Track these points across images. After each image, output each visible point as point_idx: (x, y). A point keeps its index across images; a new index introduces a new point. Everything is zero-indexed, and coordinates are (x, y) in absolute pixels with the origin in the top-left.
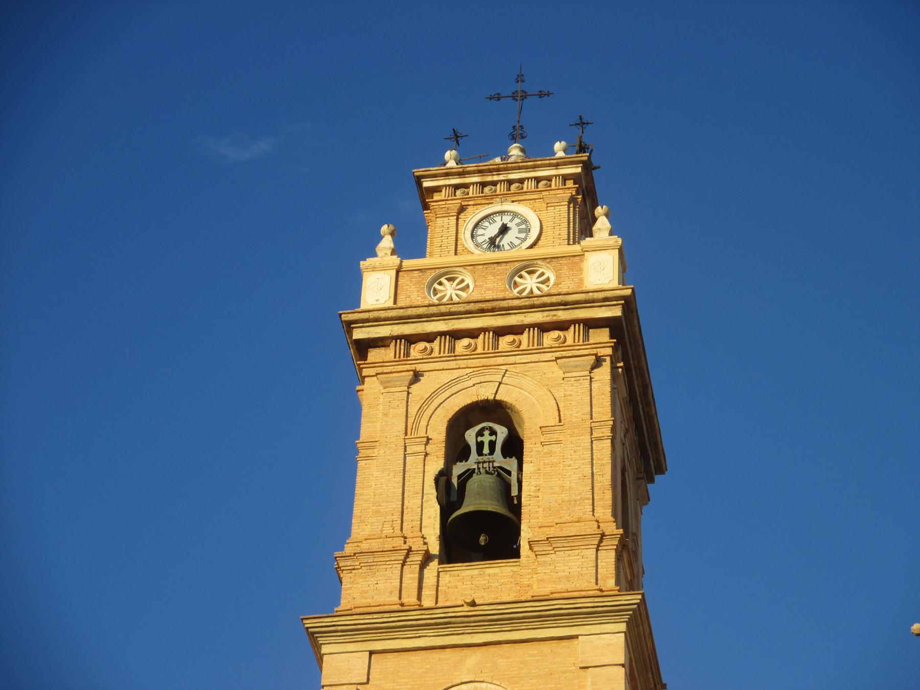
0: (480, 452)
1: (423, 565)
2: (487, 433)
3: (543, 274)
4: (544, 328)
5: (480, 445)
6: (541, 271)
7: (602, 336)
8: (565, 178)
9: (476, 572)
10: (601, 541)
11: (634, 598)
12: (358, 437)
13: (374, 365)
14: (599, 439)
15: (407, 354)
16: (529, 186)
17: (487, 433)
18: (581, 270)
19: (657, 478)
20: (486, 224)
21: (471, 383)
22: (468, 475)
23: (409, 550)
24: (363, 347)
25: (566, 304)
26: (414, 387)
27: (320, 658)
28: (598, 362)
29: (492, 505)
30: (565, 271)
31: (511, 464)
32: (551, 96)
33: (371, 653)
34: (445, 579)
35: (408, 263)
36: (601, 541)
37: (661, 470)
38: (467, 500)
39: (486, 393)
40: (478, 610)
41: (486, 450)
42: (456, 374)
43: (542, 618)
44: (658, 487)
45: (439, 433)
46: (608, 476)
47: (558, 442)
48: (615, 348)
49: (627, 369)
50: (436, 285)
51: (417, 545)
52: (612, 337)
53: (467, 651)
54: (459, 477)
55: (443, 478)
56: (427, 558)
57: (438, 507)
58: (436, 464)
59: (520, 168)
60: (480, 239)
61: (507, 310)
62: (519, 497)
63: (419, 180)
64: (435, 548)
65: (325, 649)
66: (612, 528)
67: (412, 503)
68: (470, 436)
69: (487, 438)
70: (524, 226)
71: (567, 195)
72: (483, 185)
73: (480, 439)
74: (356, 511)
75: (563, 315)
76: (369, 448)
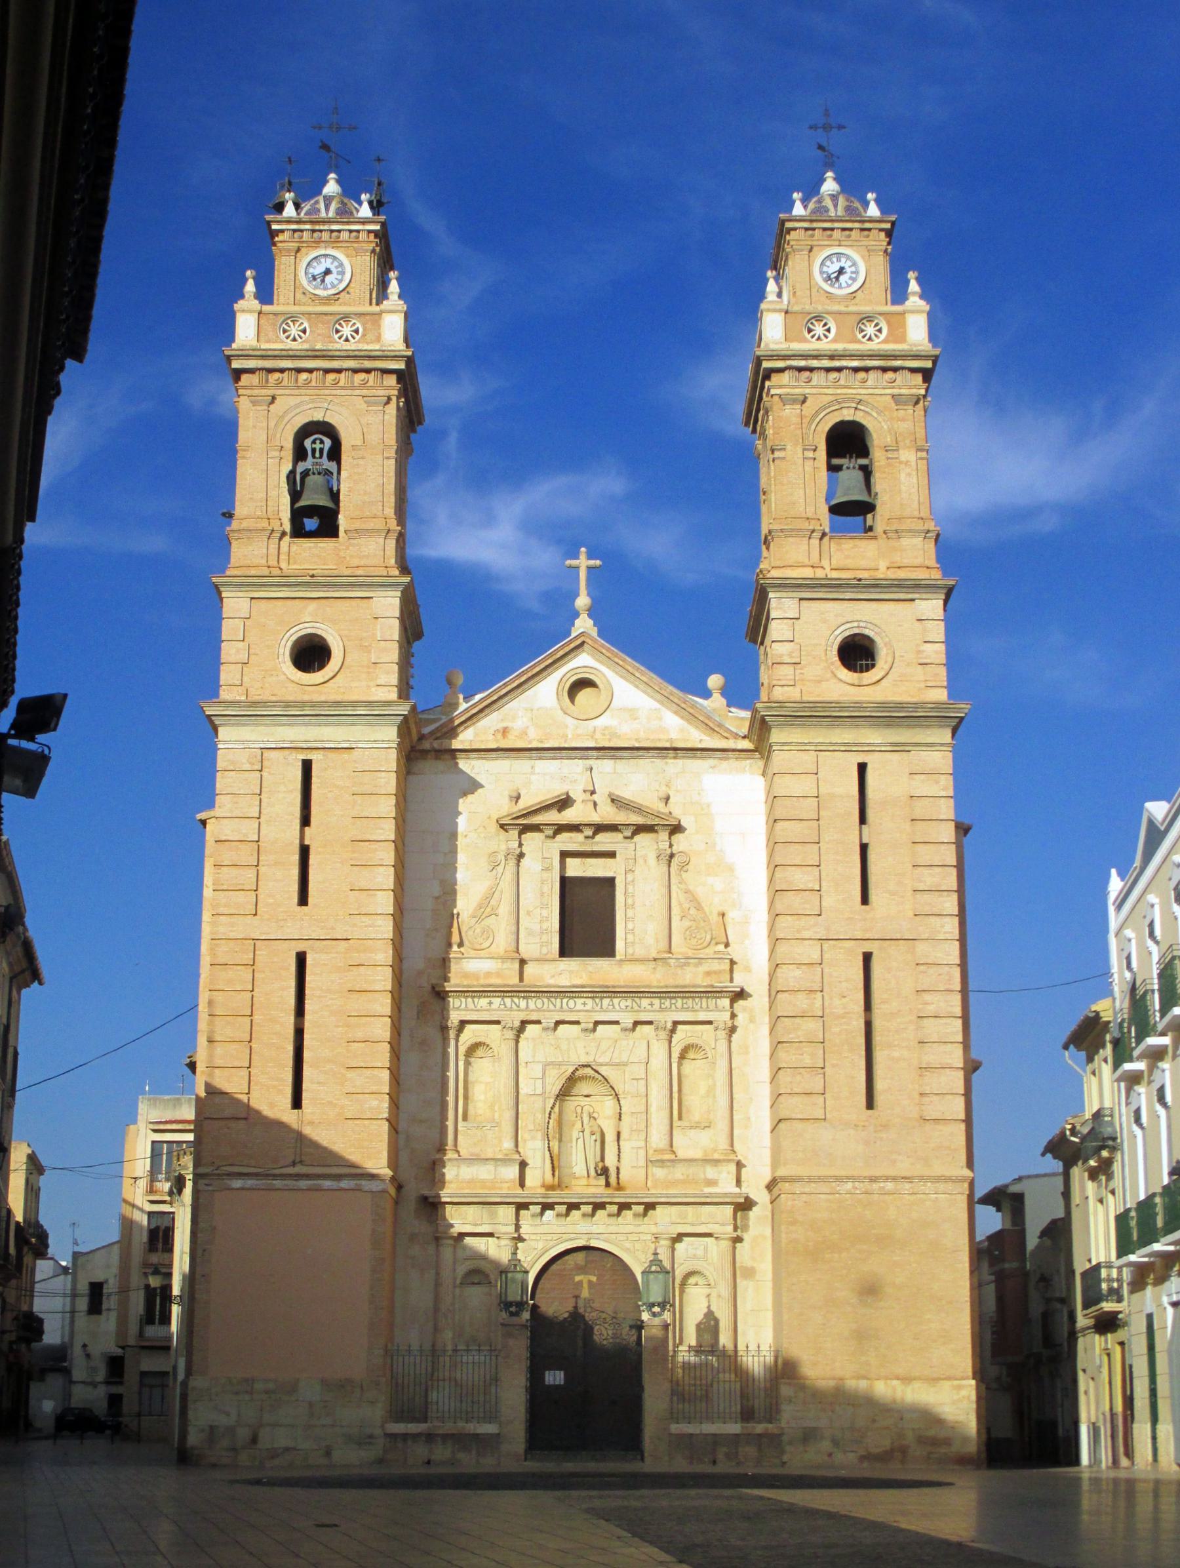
0: (314, 456)
1: (280, 539)
2: (318, 442)
3: (354, 324)
4: (356, 371)
5: (314, 450)
6: (353, 321)
7: (392, 380)
8: (369, 232)
9: (312, 545)
10: (388, 533)
11: (406, 579)
12: (237, 442)
13: (244, 387)
14: (388, 458)
15: (267, 381)
16: (344, 236)
17: (318, 442)
18: (379, 326)
20: (315, 264)
21: (308, 407)
22: (305, 474)
23: (273, 531)
24: (238, 374)
25: (370, 357)
26: (272, 407)
27: (221, 599)
28: (389, 399)
29: (324, 501)
30: (369, 326)
31: (332, 466)
33: (252, 598)
34: (294, 548)
35: (266, 308)
36: (388, 533)
37: (420, 423)
38: (304, 496)
39: (318, 416)
40: (433, 1470)
41: (317, 455)
42: (298, 400)
44: (412, 459)
45: (289, 444)
46: (393, 486)
47: (363, 458)
48: (399, 390)
49: (407, 402)
50: (284, 325)
51: (275, 525)
52: (398, 382)
54: (301, 473)
55: (291, 476)
56: (284, 534)
58: (287, 467)
59: (338, 222)
60: (311, 270)
61: (332, 357)
62: (339, 491)
63: (269, 223)
64: (287, 527)
65: (224, 595)
66: (393, 524)
67: (273, 493)
68: (308, 443)
69: (318, 446)
70: (340, 269)
71: (371, 246)
72: (313, 231)
73: (314, 446)
74: (238, 496)
75: (368, 364)
76: (245, 451)
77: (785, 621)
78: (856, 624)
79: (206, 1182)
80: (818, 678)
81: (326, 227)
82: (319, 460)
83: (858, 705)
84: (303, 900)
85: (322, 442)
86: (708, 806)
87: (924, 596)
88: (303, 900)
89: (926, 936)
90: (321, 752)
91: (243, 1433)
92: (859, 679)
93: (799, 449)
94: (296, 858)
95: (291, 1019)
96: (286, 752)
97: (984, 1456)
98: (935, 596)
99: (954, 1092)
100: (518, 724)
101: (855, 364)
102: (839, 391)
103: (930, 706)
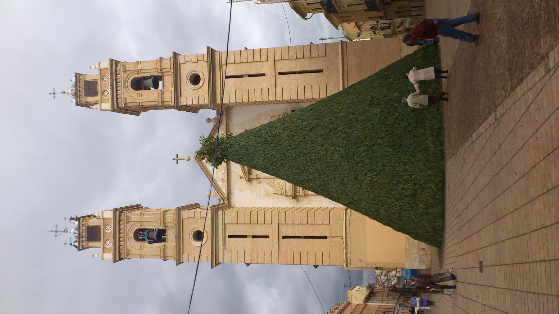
0: (144, 236)
2: (140, 235)
5: (142, 236)
13: (124, 256)
17: (140, 235)
19: (142, 206)
31: (147, 231)
32: (217, 169)
37: (140, 205)
41: (143, 235)
43: (179, 224)
53: (184, 237)
55: (150, 243)
57: (155, 243)
68: (141, 238)
77: (187, 100)
78: (187, 80)
79: (348, 264)
80: (203, 91)
81: (81, 234)
82: (145, 235)
83: (209, 79)
84: (268, 237)
85: (140, 234)
86: (242, 122)
87: (178, 61)
88: (268, 237)
89: (273, 57)
90: (226, 232)
91: (421, 252)
92: (202, 79)
93: (139, 98)
94: (255, 239)
95: (301, 239)
96: (226, 243)
97: (430, 306)
98: (178, 58)
99: (317, 47)
100: (221, 176)
101: (115, 83)
102: (123, 87)
103: (208, 58)
